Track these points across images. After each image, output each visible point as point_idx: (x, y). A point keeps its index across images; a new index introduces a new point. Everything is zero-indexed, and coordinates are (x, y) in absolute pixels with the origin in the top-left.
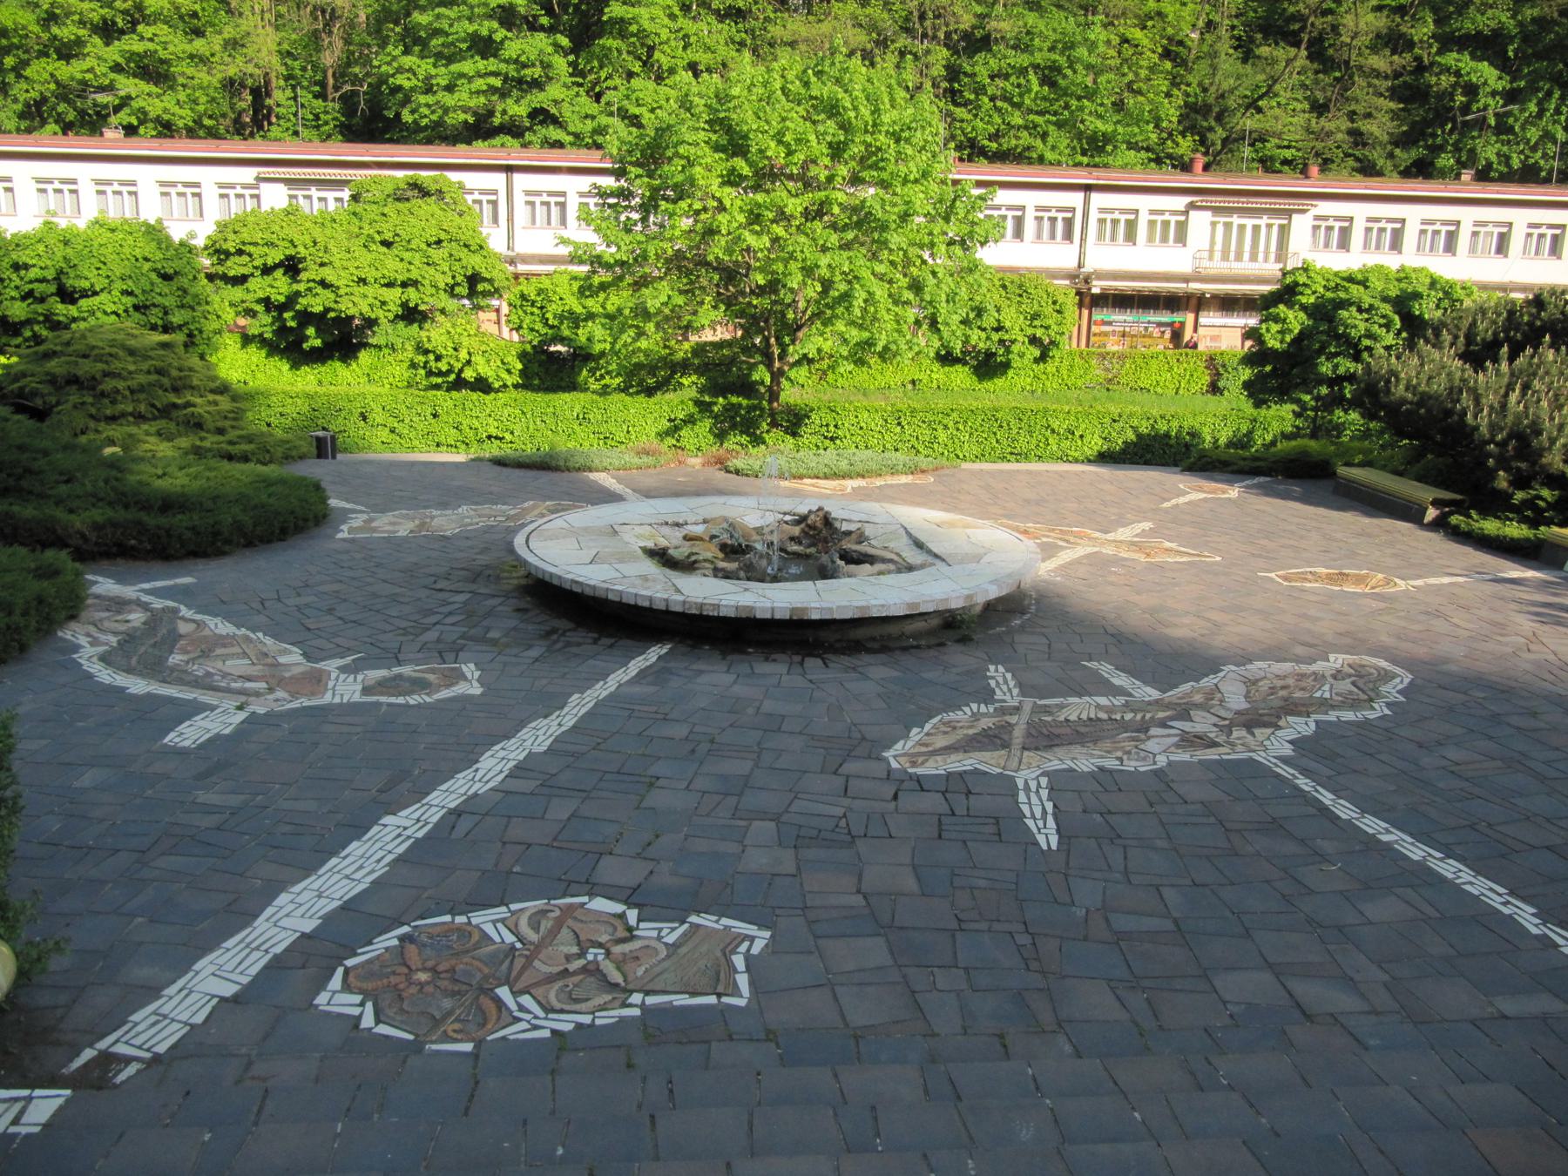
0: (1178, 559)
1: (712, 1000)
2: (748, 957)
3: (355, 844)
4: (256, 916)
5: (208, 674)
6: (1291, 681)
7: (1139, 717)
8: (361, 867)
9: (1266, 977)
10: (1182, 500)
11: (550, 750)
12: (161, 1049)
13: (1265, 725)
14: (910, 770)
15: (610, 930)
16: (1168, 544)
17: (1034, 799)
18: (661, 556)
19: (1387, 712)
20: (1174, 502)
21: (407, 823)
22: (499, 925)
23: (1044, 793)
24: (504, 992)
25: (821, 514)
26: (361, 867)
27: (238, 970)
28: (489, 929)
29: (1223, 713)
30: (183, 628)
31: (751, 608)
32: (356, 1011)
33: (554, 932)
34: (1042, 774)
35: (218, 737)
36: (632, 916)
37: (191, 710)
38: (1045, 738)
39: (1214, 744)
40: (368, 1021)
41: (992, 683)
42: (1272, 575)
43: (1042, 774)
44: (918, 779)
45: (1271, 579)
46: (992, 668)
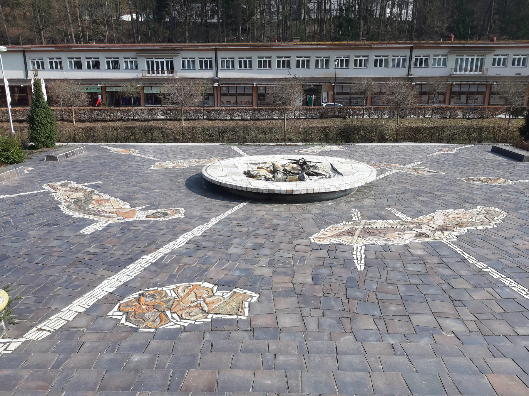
0: (429, 174)
1: (235, 317)
2: (250, 303)
3: (132, 264)
4: (96, 287)
5: (99, 211)
6: (462, 216)
7: (402, 227)
8: (133, 272)
9: (431, 318)
10: (434, 154)
11: (201, 236)
12: (57, 328)
13: (448, 230)
14: (317, 243)
15: (206, 292)
16: (426, 169)
17: (359, 253)
18: (248, 174)
19: (495, 226)
20: (431, 155)
21: (150, 258)
22: (172, 291)
23: (363, 252)
24: (168, 313)
25: (303, 160)
26: (133, 272)
27: (86, 304)
28: (168, 292)
29: (433, 226)
30: (95, 197)
31: (273, 190)
32: (120, 318)
33: (188, 294)
34: (363, 245)
35: (98, 230)
36: (215, 288)
37: (90, 222)
38: (366, 233)
39: (428, 236)
40: (123, 321)
41: (353, 215)
42: (462, 179)
43: (363, 245)
44: (320, 246)
45: (462, 181)
46: (354, 210)
